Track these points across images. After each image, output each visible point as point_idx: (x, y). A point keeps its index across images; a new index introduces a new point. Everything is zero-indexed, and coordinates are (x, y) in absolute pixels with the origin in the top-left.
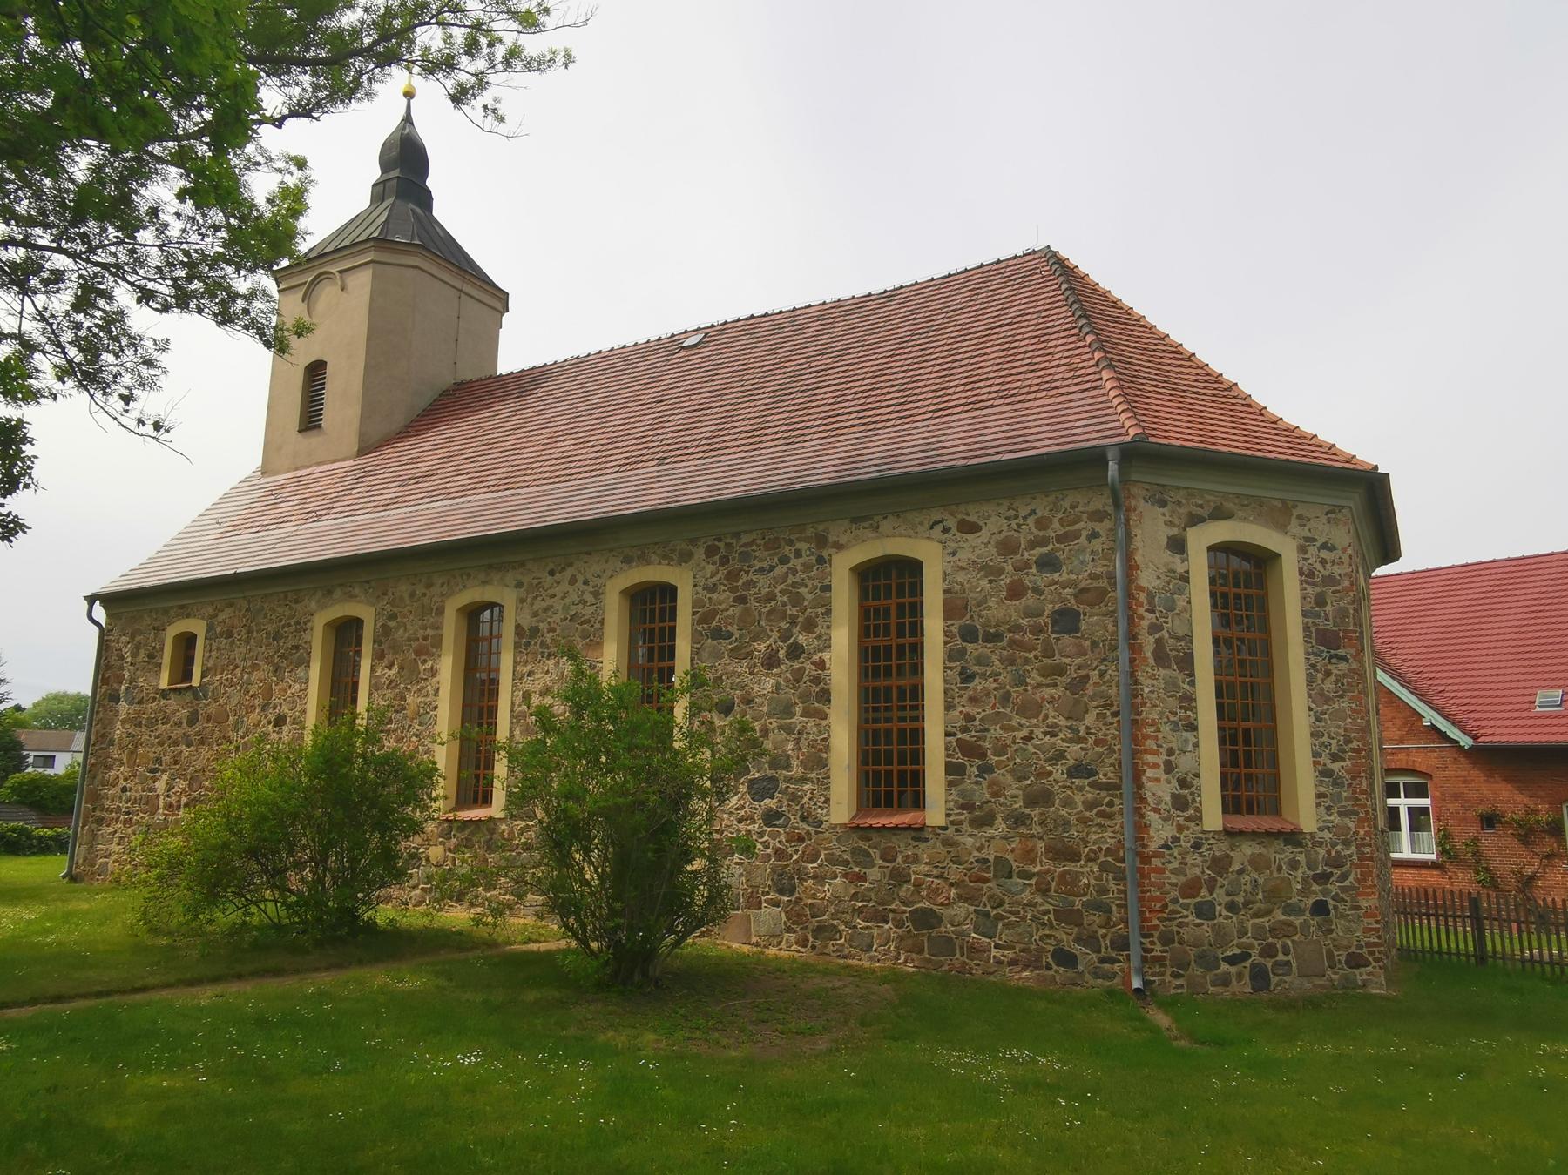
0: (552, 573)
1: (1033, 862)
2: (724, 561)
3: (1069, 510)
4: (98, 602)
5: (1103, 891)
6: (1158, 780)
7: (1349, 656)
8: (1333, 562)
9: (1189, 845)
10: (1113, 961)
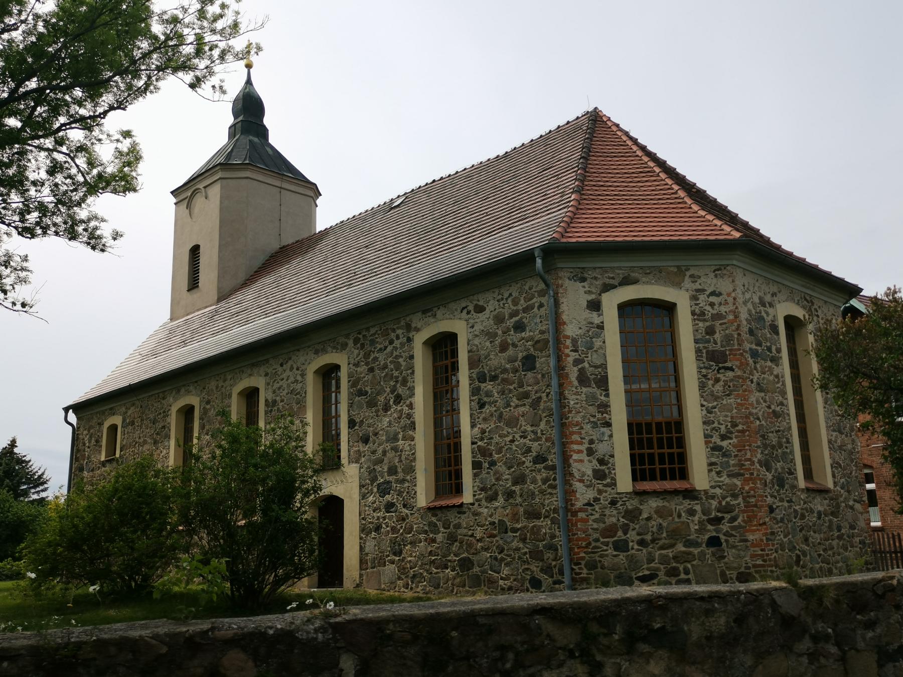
0: (282, 365)
1: (518, 521)
5: (553, 537)
6: (582, 461)
7: (734, 367)
8: (720, 304)
9: (607, 503)
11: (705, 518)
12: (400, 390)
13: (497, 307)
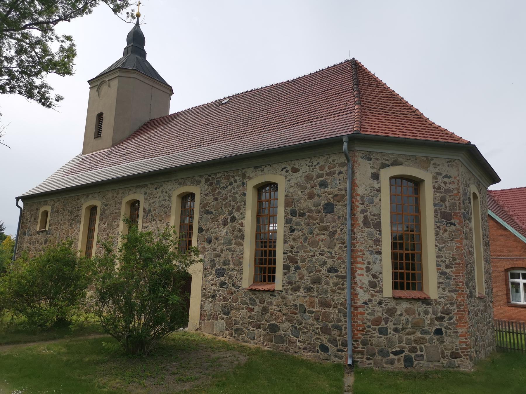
0: (156, 189)
1: (313, 307)
2: (211, 184)
3: (332, 162)
4: (20, 200)
5: (339, 321)
6: (362, 275)
7: (456, 223)
8: (450, 183)
9: (376, 303)
10: (342, 351)
11: (434, 316)
12: (236, 214)
13: (308, 170)
